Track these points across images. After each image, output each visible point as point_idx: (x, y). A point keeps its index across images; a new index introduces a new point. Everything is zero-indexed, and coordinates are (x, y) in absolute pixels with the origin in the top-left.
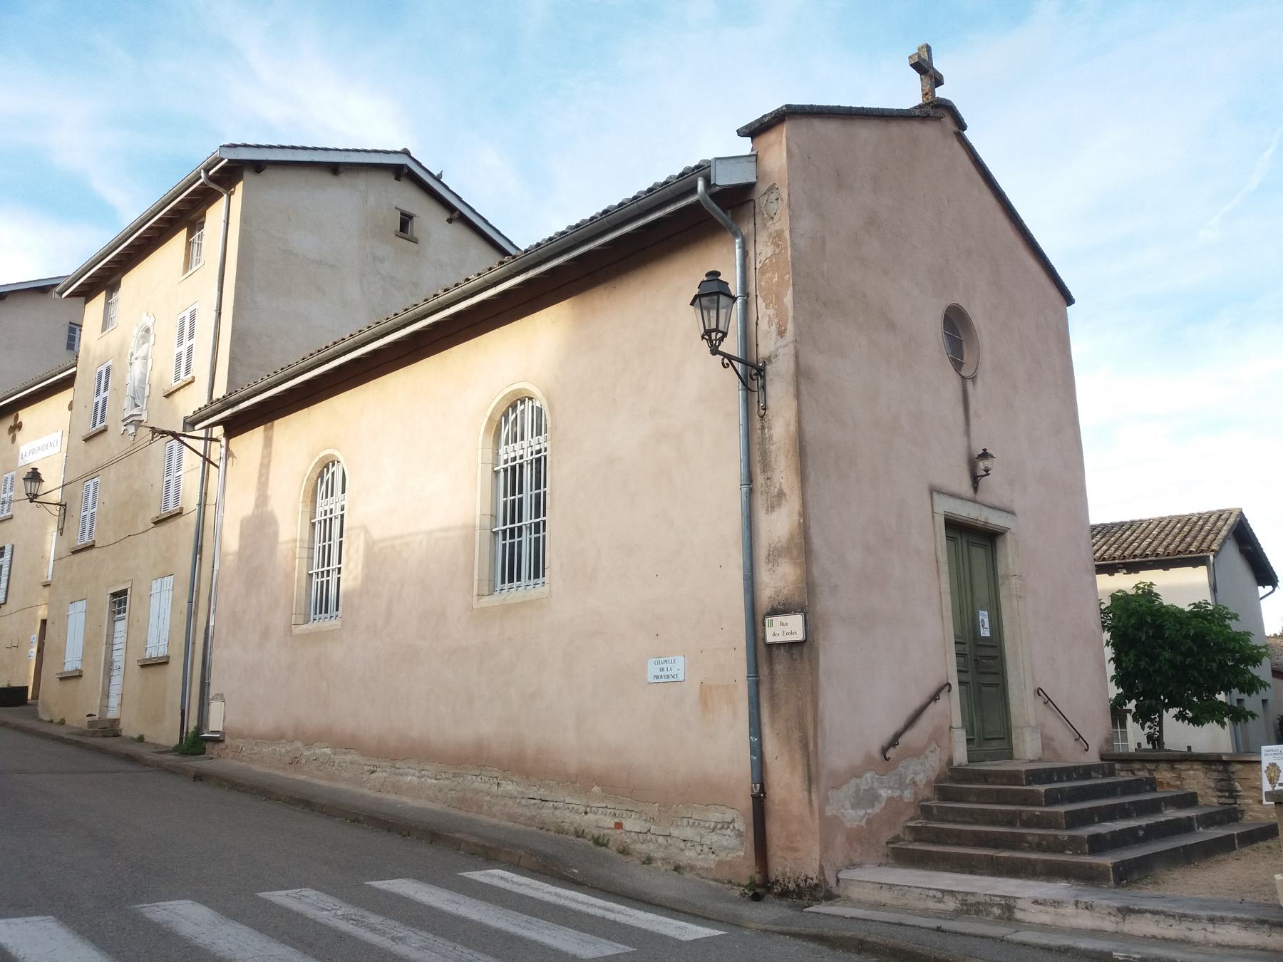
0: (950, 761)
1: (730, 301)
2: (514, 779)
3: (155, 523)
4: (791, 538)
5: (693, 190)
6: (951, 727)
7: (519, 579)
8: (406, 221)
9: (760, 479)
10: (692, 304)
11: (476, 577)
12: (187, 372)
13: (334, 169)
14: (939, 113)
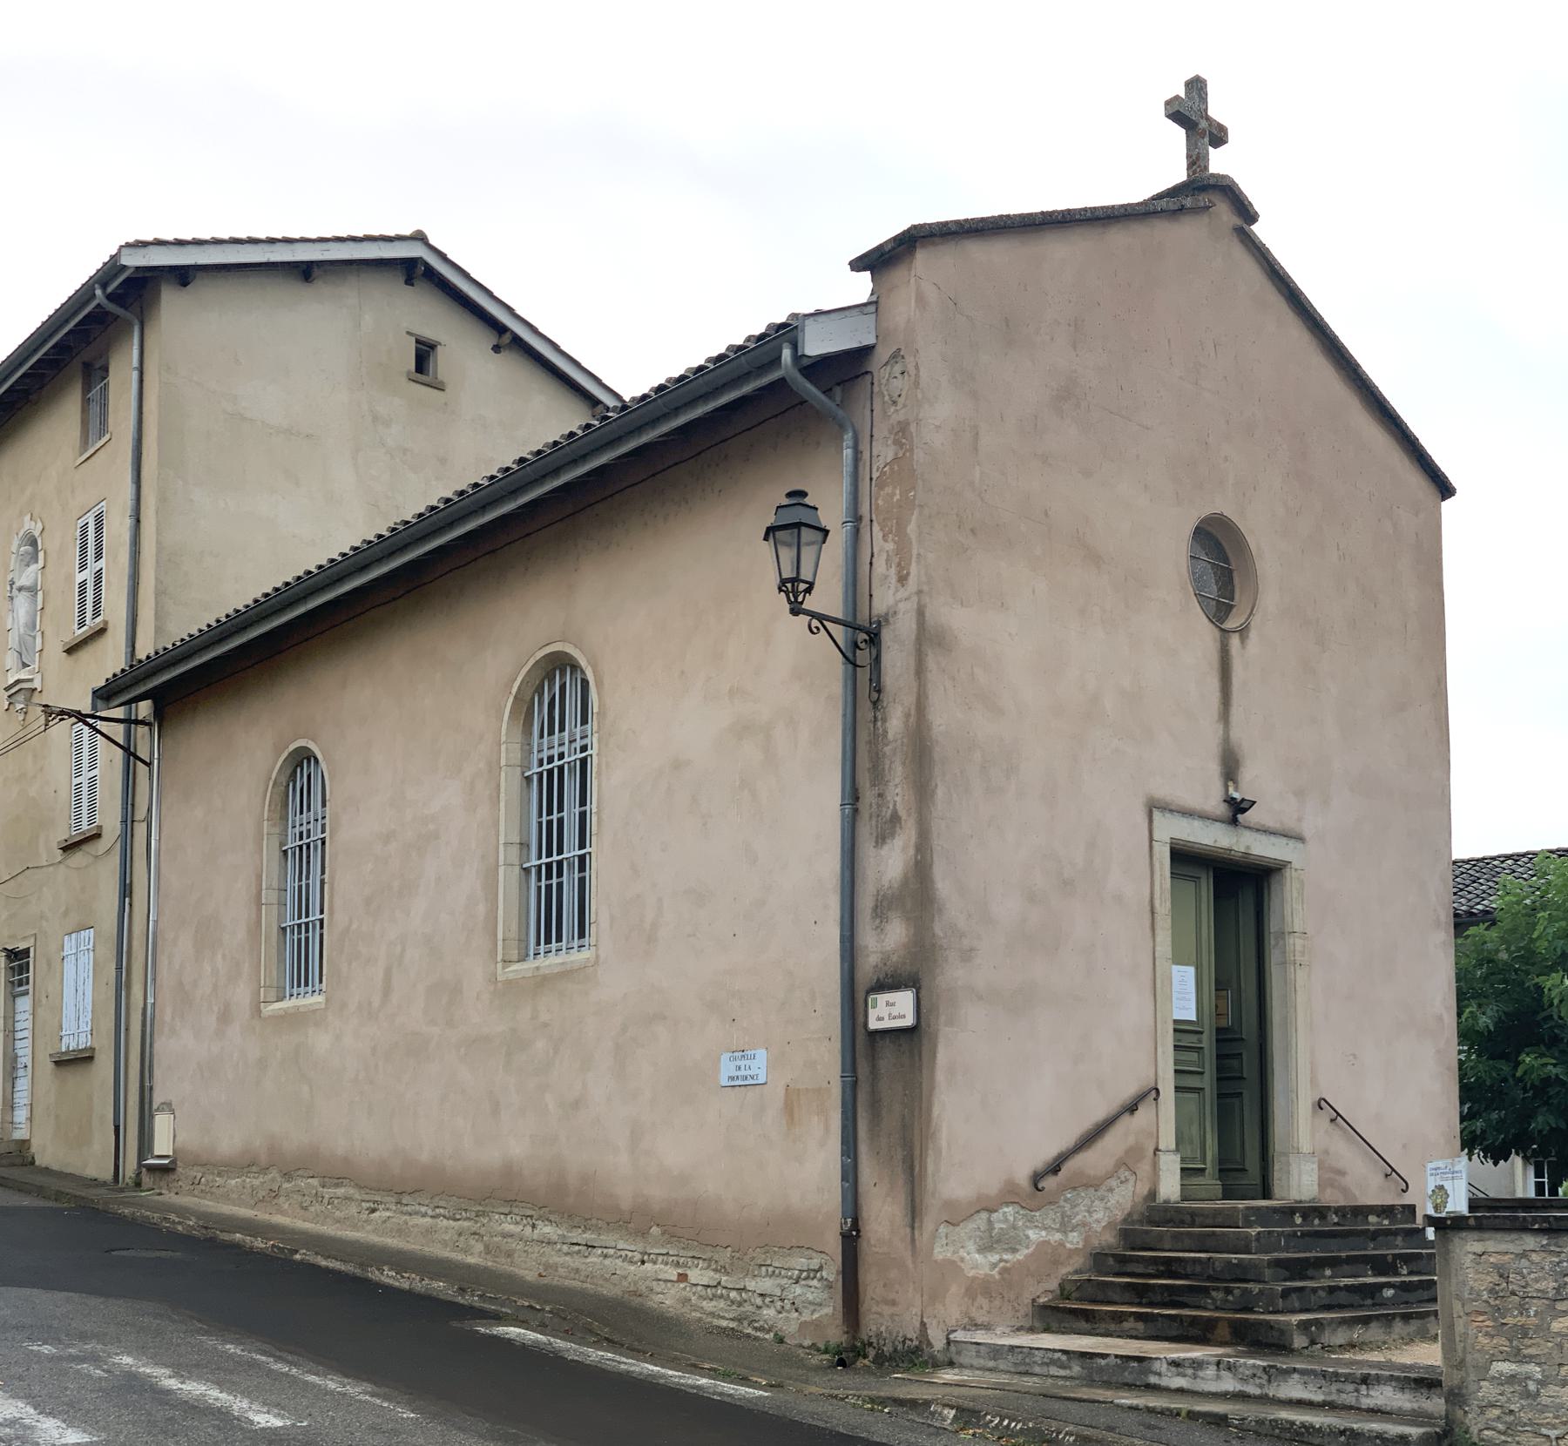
0: (1153, 1194)
1: (820, 536)
2: (552, 1217)
3: (65, 849)
4: (905, 882)
5: (776, 361)
6: (1157, 1149)
7: (559, 939)
8: (424, 354)
9: (868, 796)
10: (766, 539)
11: (500, 936)
12: (96, 613)
13: (306, 272)
14: (1207, 198)
